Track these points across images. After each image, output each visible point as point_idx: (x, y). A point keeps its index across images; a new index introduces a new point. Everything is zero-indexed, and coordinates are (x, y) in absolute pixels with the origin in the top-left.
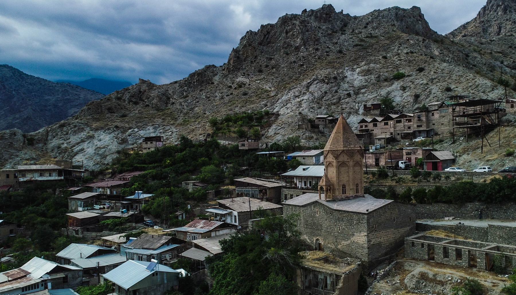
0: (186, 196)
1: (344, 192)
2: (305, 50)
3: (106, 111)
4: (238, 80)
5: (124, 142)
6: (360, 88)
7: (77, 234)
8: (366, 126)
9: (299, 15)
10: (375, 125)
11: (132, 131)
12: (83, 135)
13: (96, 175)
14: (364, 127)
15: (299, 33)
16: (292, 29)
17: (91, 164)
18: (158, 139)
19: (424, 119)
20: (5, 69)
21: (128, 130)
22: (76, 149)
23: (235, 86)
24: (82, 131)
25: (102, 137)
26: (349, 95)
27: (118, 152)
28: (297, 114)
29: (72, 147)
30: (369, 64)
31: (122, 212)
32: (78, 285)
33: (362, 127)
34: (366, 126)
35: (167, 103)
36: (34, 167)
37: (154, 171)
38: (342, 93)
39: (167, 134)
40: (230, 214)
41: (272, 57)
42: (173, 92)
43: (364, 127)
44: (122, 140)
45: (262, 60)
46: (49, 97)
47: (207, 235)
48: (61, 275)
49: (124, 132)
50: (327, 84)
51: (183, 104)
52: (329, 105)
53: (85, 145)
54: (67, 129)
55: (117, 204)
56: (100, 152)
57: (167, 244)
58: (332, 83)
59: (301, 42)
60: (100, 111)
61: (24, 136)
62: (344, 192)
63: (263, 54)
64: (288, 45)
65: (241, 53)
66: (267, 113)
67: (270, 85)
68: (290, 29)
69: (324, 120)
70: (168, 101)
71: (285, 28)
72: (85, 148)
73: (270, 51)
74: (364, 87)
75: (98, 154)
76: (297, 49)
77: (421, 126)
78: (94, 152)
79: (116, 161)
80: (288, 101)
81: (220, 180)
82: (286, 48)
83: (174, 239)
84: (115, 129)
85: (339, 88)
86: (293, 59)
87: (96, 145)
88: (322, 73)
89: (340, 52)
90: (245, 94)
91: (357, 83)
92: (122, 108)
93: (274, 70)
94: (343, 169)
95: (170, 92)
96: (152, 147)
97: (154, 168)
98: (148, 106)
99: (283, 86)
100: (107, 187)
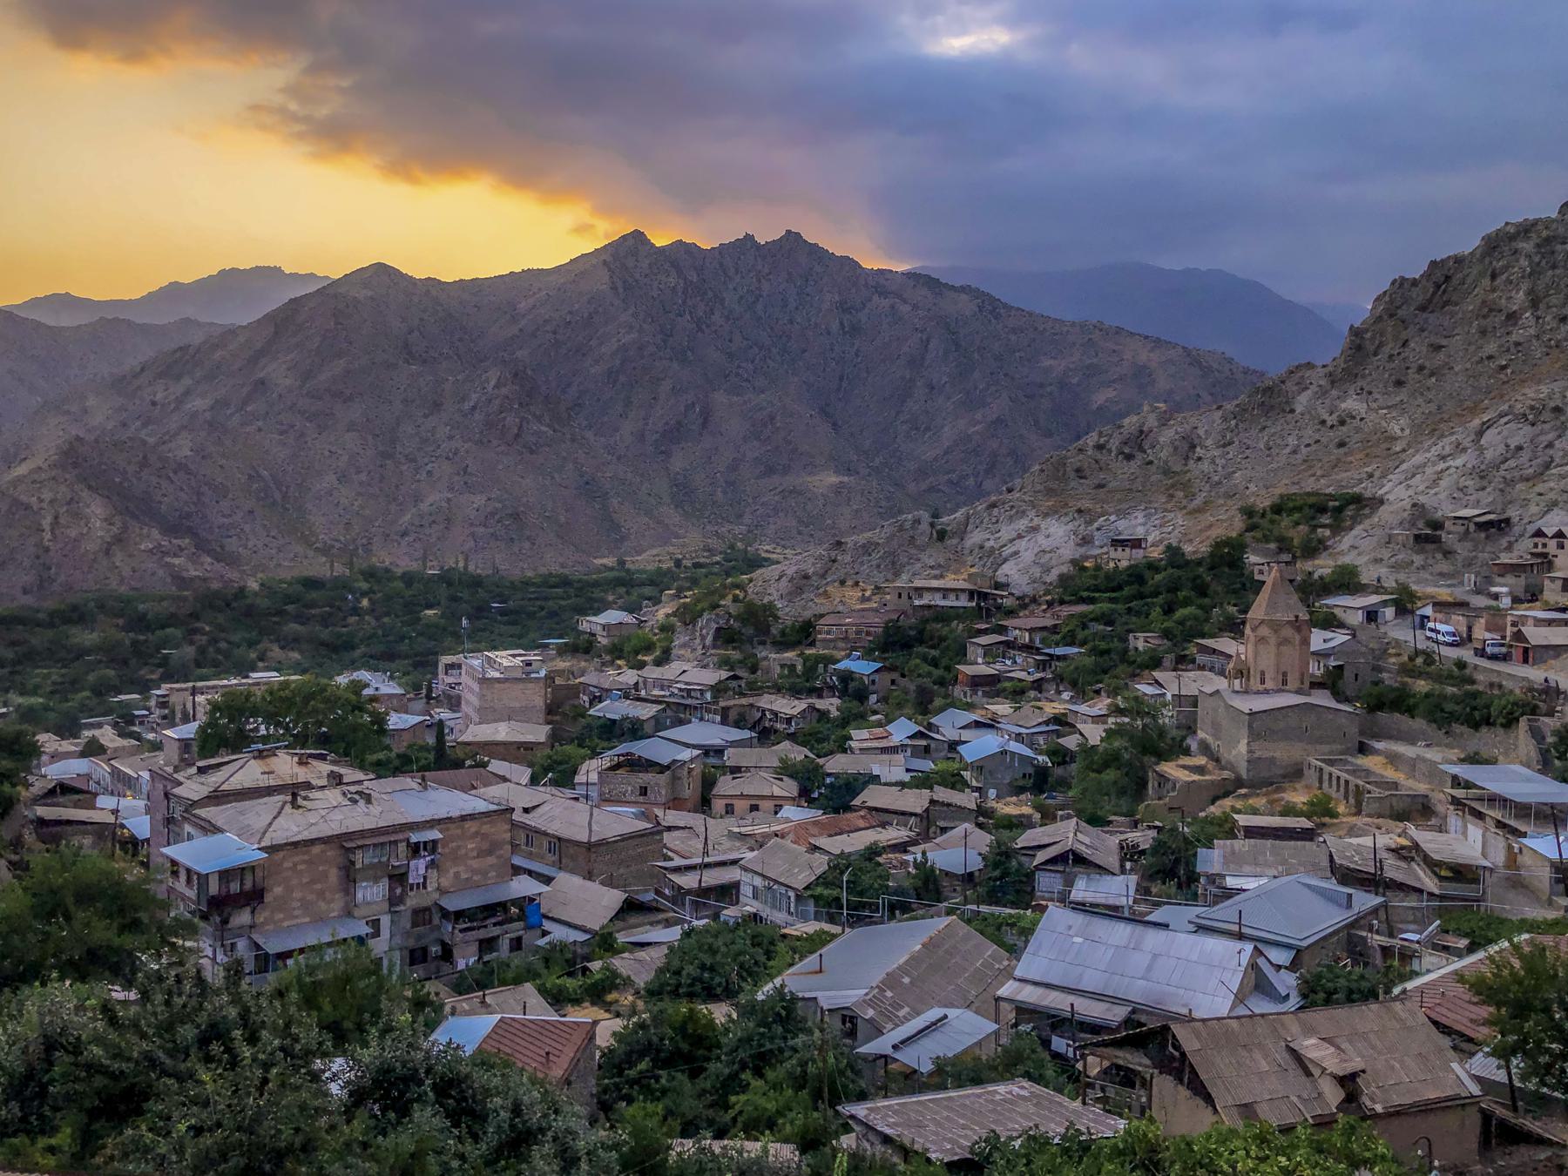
1: (1263, 682)
2: (1532, 322)
3: (1072, 475)
4: (1343, 406)
8: (1545, 545)
9: (1553, 221)
12: (1022, 524)
13: (1026, 603)
16: (1506, 268)
17: (1024, 580)
18: (1136, 544)
20: (964, 297)
22: (1007, 551)
23: (1331, 420)
25: (1052, 530)
27: (1074, 562)
33: (1536, 546)
36: (935, 583)
37: (1104, 606)
41: (1444, 342)
45: (1418, 348)
46: (1052, 362)
48: (924, 743)
49: (1090, 522)
53: (1022, 545)
57: (1047, 723)
61: (932, 525)
62: (1263, 682)
65: (1369, 335)
66: (1357, 500)
76: (1512, 317)
80: (1419, 468)
81: (1194, 631)
82: (1484, 317)
86: (1491, 347)
90: (1342, 445)
94: (1261, 647)
95: (1201, 432)
96: (1124, 559)
97: (1111, 600)
98: (1151, 463)
99: (1430, 428)
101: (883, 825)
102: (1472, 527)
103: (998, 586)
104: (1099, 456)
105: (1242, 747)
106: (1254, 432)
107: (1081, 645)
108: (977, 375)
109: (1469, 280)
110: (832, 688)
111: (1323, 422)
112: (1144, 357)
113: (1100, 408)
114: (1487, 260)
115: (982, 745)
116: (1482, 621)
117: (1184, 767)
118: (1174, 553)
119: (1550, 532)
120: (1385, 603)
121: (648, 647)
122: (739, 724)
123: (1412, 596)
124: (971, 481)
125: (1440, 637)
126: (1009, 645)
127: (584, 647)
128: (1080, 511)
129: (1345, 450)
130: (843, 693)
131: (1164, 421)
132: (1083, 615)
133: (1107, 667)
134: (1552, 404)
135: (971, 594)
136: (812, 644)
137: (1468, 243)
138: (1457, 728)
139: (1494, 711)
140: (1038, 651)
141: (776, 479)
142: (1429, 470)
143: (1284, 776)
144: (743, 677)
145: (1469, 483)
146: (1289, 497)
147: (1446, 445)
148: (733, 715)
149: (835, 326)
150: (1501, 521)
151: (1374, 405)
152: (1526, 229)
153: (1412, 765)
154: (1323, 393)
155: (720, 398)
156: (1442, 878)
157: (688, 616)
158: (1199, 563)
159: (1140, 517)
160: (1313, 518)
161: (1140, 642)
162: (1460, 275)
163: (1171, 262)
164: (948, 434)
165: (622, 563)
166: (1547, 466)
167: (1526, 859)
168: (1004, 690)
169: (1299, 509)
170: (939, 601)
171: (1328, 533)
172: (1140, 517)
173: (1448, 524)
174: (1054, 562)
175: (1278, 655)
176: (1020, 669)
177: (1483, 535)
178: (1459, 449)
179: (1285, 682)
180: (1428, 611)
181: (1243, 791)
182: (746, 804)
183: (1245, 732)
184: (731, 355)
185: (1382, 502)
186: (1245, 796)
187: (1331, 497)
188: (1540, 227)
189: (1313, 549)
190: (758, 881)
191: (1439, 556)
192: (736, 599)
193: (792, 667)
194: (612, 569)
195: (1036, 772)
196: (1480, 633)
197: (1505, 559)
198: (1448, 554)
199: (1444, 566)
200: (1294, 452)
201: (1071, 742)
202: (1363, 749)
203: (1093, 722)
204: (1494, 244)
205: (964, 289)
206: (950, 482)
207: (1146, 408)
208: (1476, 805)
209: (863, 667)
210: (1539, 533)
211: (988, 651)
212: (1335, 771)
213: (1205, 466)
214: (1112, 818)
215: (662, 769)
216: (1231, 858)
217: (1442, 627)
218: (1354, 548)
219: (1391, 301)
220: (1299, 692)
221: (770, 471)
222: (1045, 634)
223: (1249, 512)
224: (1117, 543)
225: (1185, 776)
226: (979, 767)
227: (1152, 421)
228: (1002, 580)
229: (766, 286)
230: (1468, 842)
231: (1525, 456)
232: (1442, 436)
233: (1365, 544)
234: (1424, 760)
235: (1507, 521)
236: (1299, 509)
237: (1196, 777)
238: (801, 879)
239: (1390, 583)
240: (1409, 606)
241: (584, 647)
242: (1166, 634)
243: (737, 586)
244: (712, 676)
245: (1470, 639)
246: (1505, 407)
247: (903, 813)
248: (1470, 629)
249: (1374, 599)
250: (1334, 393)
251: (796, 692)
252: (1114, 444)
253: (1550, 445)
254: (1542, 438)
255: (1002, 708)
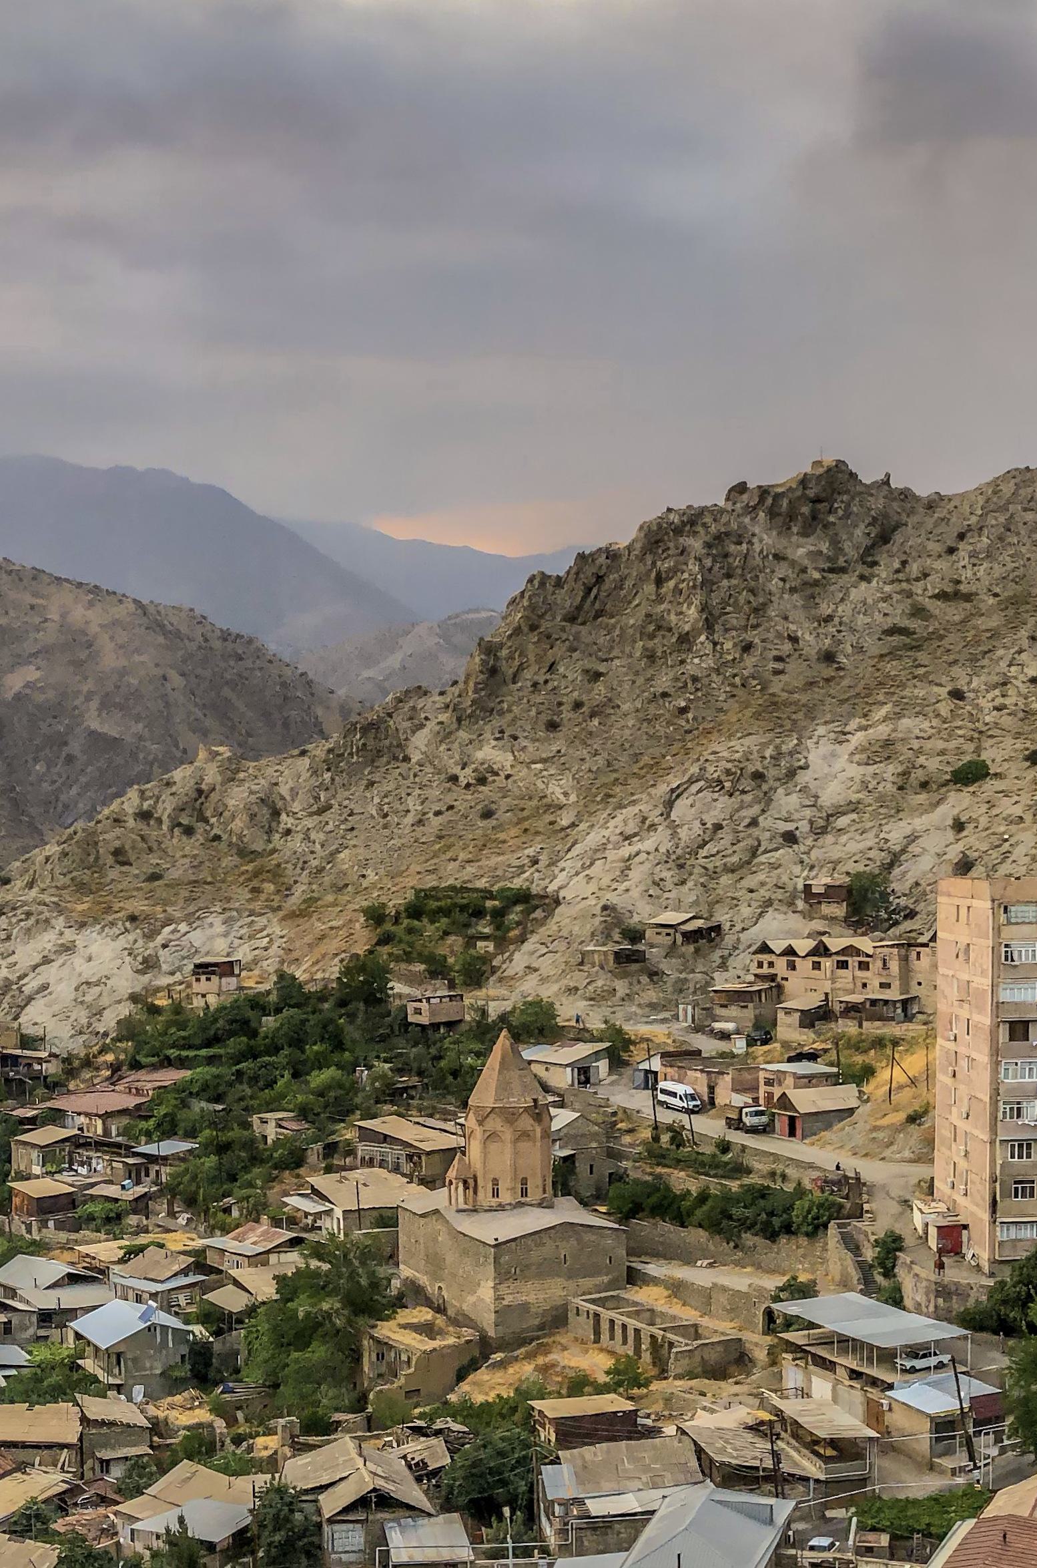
0: (255, 1153)
1: (496, 1194)
3: (110, 860)
5: (148, 967)
7: (29, 1232)
8: (771, 964)
10: (792, 966)
11: (173, 932)
12: (47, 940)
13: (73, 1067)
14: (765, 965)
15: (694, 587)
18: (226, 969)
19: (894, 966)
21: (163, 927)
22: (31, 985)
23: (466, 776)
24: (45, 930)
27: (134, 998)
28: (598, 910)
29: (20, 978)
30: (899, 716)
31: (123, 1187)
32: (28, 1341)
34: (771, 964)
35: (269, 832)
38: (772, 823)
39: (258, 943)
40: (329, 1213)
41: (602, 668)
42: (292, 789)
43: (765, 965)
44: (145, 961)
47: (259, 1260)
49: (150, 936)
50: (731, 795)
51: (313, 836)
52: (714, 875)
53: (49, 974)
54: (10, 924)
55: (114, 1164)
56: (88, 998)
57: (185, 1272)
58: (743, 792)
59: (697, 621)
60: (92, 858)
62: (496, 1194)
63: (576, 655)
64: (659, 628)
66: (523, 897)
67: (567, 781)
68: (669, 569)
69: (671, 931)
70: (274, 824)
71: (654, 563)
72: (52, 982)
73: (601, 641)
75: (82, 1003)
76: (685, 640)
77: (888, 986)
78: (73, 996)
79: (128, 1030)
81: (340, 1105)
83: (200, 1263)
84: (128, 924)
85: (763, 811)
86: (664, 681)
87: (80, 975)
89: (829, 657)
90: (487, 814)
92: (150, 849)
93: (596, 722)
95: (284, 790)
96: (210, 995)
97: (211, 1060)
98: (217, 838)
99: (602, 794)
100: (96, 1115)
102: (679, 939)
103: (27, 1042)
104: (146, 831)
106: (358, 790)
107: (191, 1134)
109: (629, 583)
111: (454, 779)
112: (79, 614)
113: (18, 697)
114: (649, 559)
116: (728, 1078)
117: (405, 1327)
119: (778, 946)
120: (597, 1055)
125: (676, 1102)
126: (79, 1142)
128: (133, 918)
129: (492, 822)
131: (231, 775)
134: (751, 768)
138: (748, 1239)
139: (796, 1215)
140: (129, 1151)
142: (612, 855)
143: (541, 1327)
145: (666, 874)
147: (626, 819)
150: (711, 929)
151: (522, 756)
152: (692, 520)
153: (706, 1298)
154: (445, 735)
156: (827, 1460)
158: (322, 997)
159: (216, 923)
160: (467, 926)
161: (271, 1127)
162: (614, 576)
166: (754, 852)
167: (896, 1419)
168: (91, 1218)
169: (446, 912)
171: (490, 946)
172: (216, 923)
173: (648, 933)
174: (105, 1001)
175: (516, 1153)
176: (103, 1179)
177: (691, 948)
178: (646, 826)
179: (524, 1193)
180: (656, 1064)
181: (498, 1356)
183: (491, 1269)
185: (557, 902)
186: (502, 1365)
187: (488, 894)
188: (708, 519)
191: (645, 979)
195: (191, 1351)
196: (727, 1096)
197: (723, 982)
198: (654, 975)
200: (420, 822)
201: (228, 1299)
202: (633, 1277)
204: (659, 537)
207: (202, 755)
208: (822, 1352)
210: (765, 949)
211: (48, 1153)
212: (612, 1314)
213: (296, 843)
214: (337, 1417)
216: (584, 1474)
217: (680, 1089)
218: (532, 972)
219: (532, 607)
220: (543, 1204)
222: (125, 1121)
223: (376, 916)
224: (204, 969)
225: (418, 1344)
226: (115, 1357)
227: (212, 775)
228: (29, 1031)
231: (726, 836)
232: (621, 806)
233: (546, 965)
234: (724, 1289)
235: (718, 929)
236: (446, 912)
237: (431, 1345)
240: (625, 1056)
242: (304, 1113)
245: (712, 1102)
246: (694, 769)
247: (49, 1446)
248: (712, 1089)
249: (582, 1050)
250: (463, 735)
252: (166, 808)
253: (754, 823)
254: (744, 813)
255: (105, 1250)
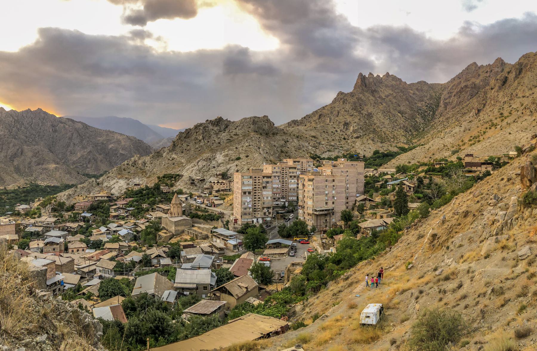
0: (142, 209)
6: (221, 164)
12: (115, 181)
13: (118, 198)
18: (139, 185)
22: (112, 187)
23: (171, 159)
26: (214, 167)
36: (99, 195)
37: (135, 199)
38: (212, 165)
45: (185, 145)
53: (115, 185)
66: (178, 175)
67: (184, 160)
74: (223, 163)
76: (200, 141)
79: (125, 193)
81: (154, 203)
86: (197, 146)
88: (205, 156)
89: (219, 143)
90: (174, 164)
91: (220, 161)
96: (136, 188)
99: (189, 161)
101: (111, 251)
103: (112, 194)
105: (173, 228)
107: (134, 207)
108: (84, 142)
110: (81, 220)
112: (119, 137)
115: (123, 232)
118: (147, 187)
119: (212, 182)
121: (35, 214)
122: (63, 230)
123: (192, 195)
124: (85, 165)
126: (119, 208)
127: (19, 214)
130: (84, 221)
132: (132, 201)
133: (139, 213)
135: (107, 197)
136: (74, 210)
137: (192, 127)
138: (209, 221)
141: (40, 166)
144: (60, 219)
146: (165, 175)
147: (192, 165)
148: (61, 228)
149: (51, 130)
152: (201, 125)
153: (203, 229)
154: (168, 153)
155: (25, 147)
157: (44, 205)
158: (151, 188)
161: (145, 206)
163: (121, 116)
164: (79, 155)
165: (5, 188)
167: (228, 245)
170: (100, 199)
176: (122, 213)
180: (196, 197)
182: (76, 250)
184: (26, 137)
189: (172, 185)
190: (101, 269)
192: (55, 201)
193: (71, 216)
194: (2, 190)
196: (206, 202)
197: (205, 187)
198: (196, 186)
199: (196, 188)
201: (139, 229)
202: (193, 226)
203: (142, 224)
204: (196, 127)
205: (79, 122)
206: (80, 165)
209: (88, 215)
213: (148, 168)
215: (58, 244)
216: (186, 252)
218: (179, 185)
221: (39, 164)
223: (159, 178)
224: (135, 185)
226: (124, 237)
227: (137, 159)
229: (34, 121)
230: (219, 243)
231: (206, 167)
233: (181, 184)
238: (111, 267)
239: (188, 192)
241: (19, 214)
242: (149, 204)
243: (54, 198)
244: (53, 220)
249: (186, 196)
251: (73, 222)
252: (130, 163)
